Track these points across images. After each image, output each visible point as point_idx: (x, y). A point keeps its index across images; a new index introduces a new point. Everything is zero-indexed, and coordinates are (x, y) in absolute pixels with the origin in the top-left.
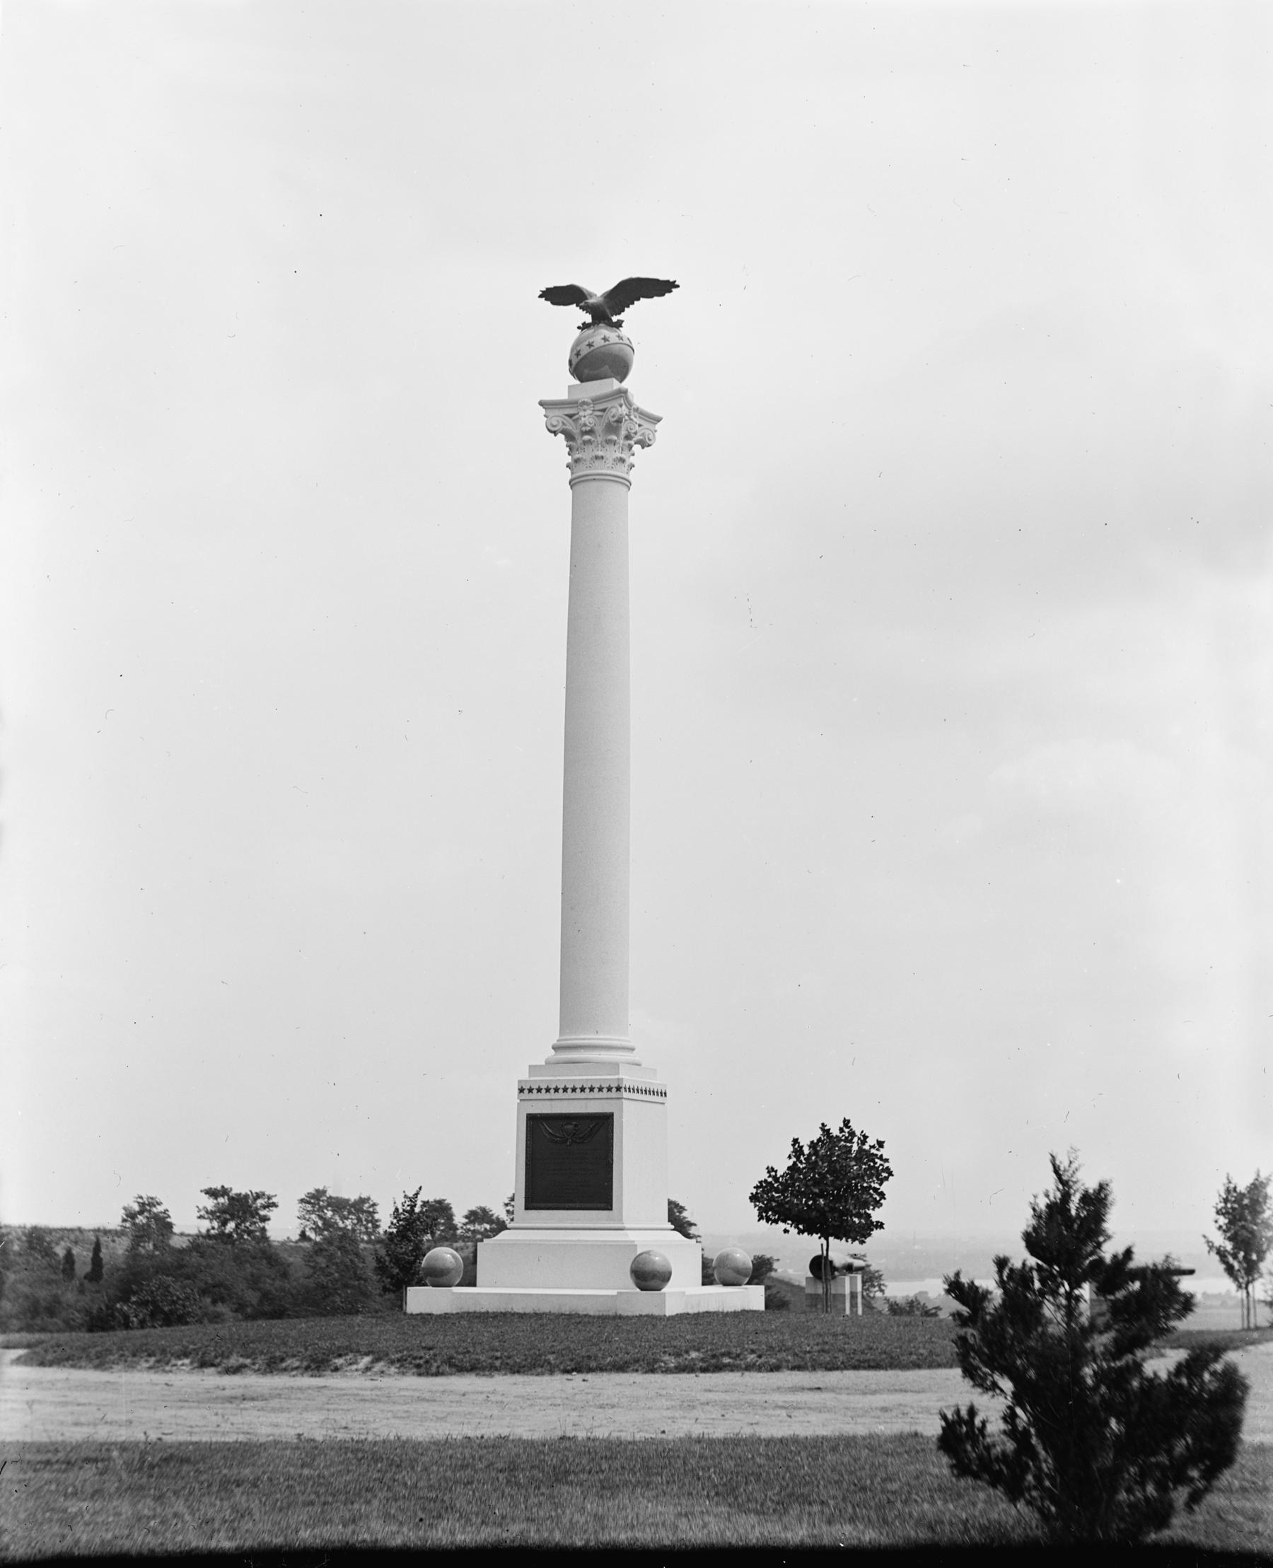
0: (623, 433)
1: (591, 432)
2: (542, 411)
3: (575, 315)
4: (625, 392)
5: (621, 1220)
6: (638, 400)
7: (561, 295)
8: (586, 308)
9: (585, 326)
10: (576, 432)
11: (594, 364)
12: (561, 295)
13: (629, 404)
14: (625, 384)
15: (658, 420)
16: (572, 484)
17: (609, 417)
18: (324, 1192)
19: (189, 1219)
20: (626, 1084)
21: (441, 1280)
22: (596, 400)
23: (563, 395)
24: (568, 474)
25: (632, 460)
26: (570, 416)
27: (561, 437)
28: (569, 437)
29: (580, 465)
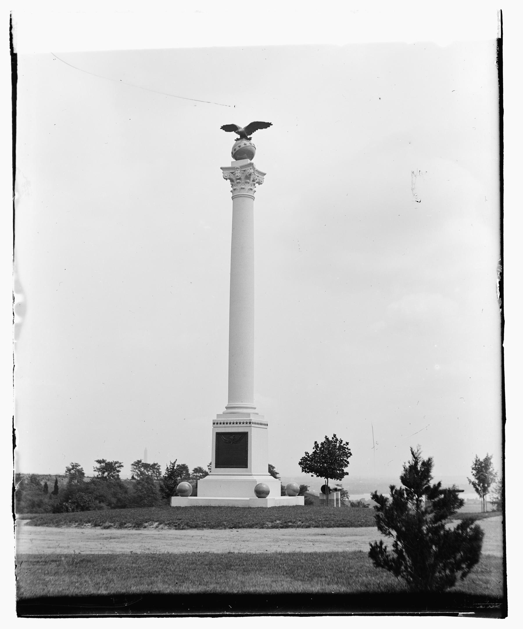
0: (252, 179)
1: (240, 179)
2: (222, 171)
3: (234, 136)
5: (251, 472)
6: (258, 167)
7: (229, 128)
8: (238, 133)
9: (237, 140)
10: (234, 179)
11: (241, 154)
12: (229, 128)
13: (254, 168)
14: (252, 161)
17: (247, 173)
19: (90, 471)
20: (254, 419)
22: (242, 167)
23: (229, 165)
24: (231, 195)
25: (255, 189)
26: (232, 173)
27: (229, 181)
28: (232, 181)
29: (236, 191)
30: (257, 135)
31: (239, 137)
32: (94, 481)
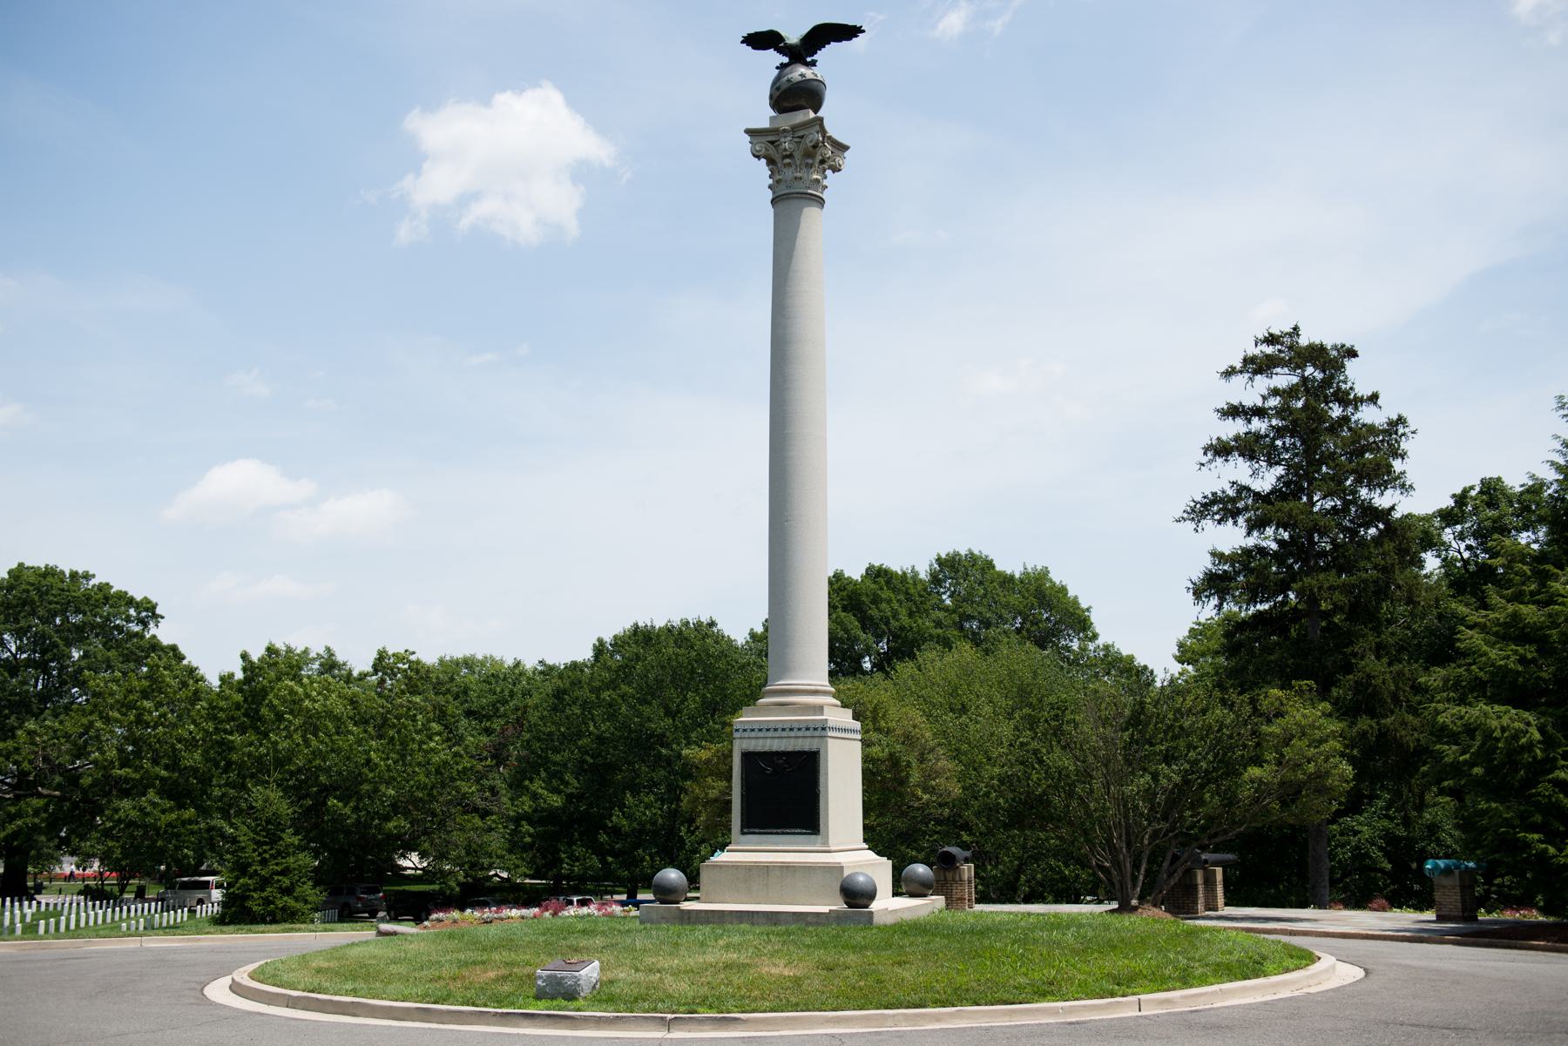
0: (819, 158)
1: (790, 156)
2: (748, 138)
3: (773, 58)
4: (821, 120)
5: (826, 843)
6: (832, 130)
7: (762, 40)
8: (780, 51)
9: (782, 67)
10: (778, 158)
11: (795, 97)
12: (762, 40)
13: (823, 131)
14: (820, 114)
15: (846, 148)
16: (773, 202)
17: (808, 142)
18: (600, 641)
19: (963, 553)
20: (830, 724)
21: (671, 898)
22: (794, 128)
23: (766, 124)
24: (769, 195)
25: (825, 182)
26: (772, 143)
27: (763, 161)
28: (771, 162)
29: (782, 186)
30: (830, 58)
31: (786, 60)
32: (1175, 689)
